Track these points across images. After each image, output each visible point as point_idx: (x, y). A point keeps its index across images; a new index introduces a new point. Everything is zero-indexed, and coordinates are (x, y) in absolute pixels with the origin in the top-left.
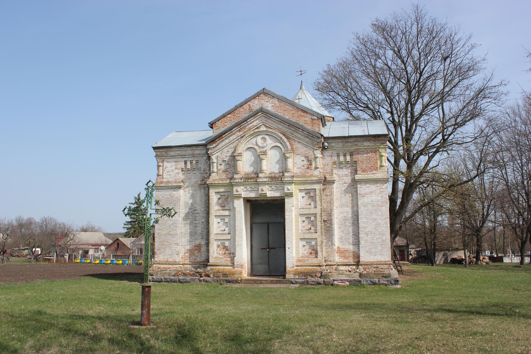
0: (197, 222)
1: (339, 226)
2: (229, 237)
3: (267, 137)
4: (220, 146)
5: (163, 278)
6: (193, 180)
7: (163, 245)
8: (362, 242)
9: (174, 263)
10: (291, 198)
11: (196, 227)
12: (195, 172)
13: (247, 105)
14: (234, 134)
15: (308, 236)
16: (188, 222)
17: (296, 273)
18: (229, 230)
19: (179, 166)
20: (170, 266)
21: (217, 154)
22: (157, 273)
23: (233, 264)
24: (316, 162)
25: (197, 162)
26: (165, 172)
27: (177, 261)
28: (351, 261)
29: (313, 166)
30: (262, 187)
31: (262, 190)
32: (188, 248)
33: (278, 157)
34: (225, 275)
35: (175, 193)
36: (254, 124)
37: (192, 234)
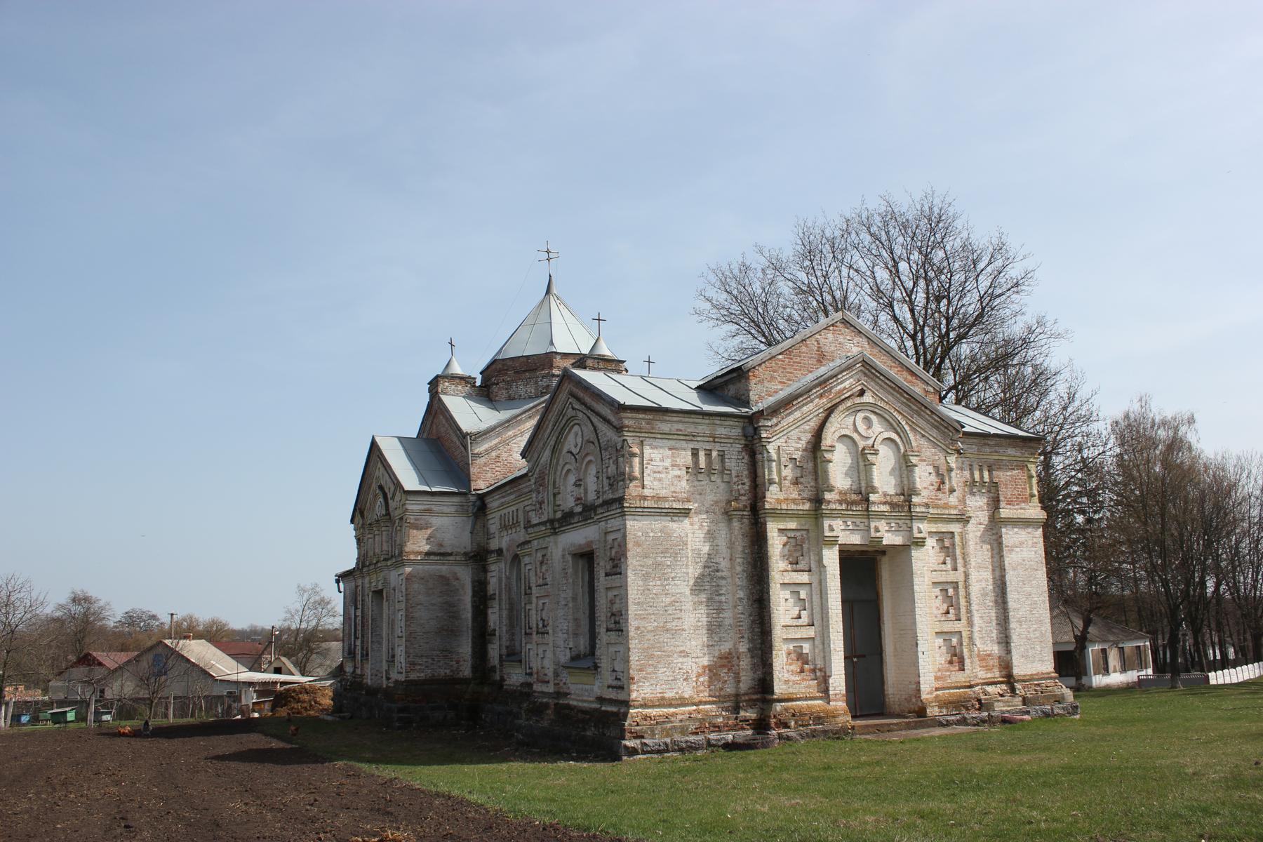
0: (723, 598)
2: (811, 632)
3: (873, 417)
4: (784, 423)
5: (668, 740)
6: (710, 498)
7: (652, 656)
8: (1014, 637)
9: (682, 702)
10: (923, 550)
11: (719, 610)
13: (813, 339)
14: (812, 401)
15: (947, 627)
16: (703, 597)
17: (944, 704)
18: (811, 615)
19: (680, 461)
20: (672, 710)
21: (778, 443)
22: (653, 731)
23: (826, 691)
24: (950, 478)
25: (722, 455)
26: (647, 472)
27: (686, 696)
28: (996, 674)
29: (947, 486)
30: (877, 524)
31: (877, 530)
32: (706, 664)
33: (893, 462)
34: (819, 720)
35: (674, 525)
36: (847, 384)
37: (714, 628)
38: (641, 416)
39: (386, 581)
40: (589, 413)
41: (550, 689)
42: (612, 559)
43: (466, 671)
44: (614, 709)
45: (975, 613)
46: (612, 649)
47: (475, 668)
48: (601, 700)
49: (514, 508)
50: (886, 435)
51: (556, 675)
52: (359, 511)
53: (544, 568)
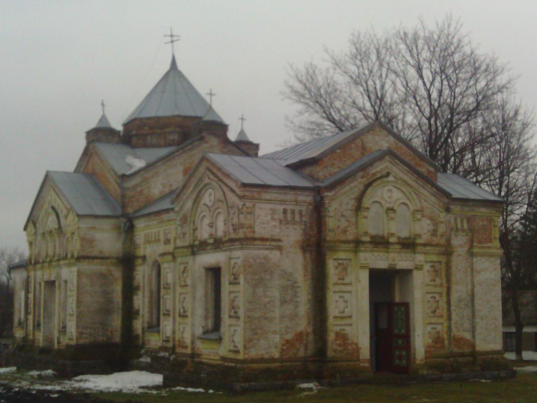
1: (296, 285)
3: (394, 189)
12: (296, 227)
17: (428, 366)
38: (254, 190)
39: (58, 276)
40: (221, 183)
41: (189, 351)
42: (234, 274)
43: (117, 338)
44: (233, 365)
45: (453, 312)
46: (233, 328)
47: (123, 336)
48: (224, 359)
49: (156, 230)
50: (402, 201)
51: (193, 343)
52: (32, 220)
53: (185, 275)
